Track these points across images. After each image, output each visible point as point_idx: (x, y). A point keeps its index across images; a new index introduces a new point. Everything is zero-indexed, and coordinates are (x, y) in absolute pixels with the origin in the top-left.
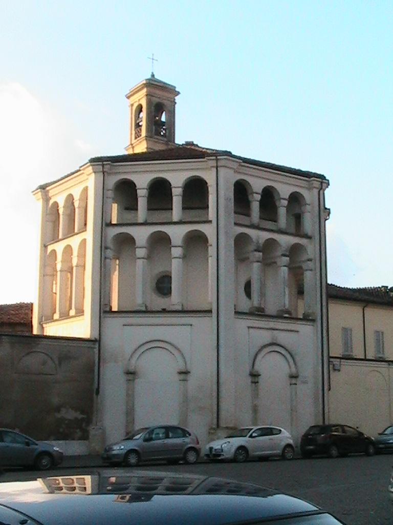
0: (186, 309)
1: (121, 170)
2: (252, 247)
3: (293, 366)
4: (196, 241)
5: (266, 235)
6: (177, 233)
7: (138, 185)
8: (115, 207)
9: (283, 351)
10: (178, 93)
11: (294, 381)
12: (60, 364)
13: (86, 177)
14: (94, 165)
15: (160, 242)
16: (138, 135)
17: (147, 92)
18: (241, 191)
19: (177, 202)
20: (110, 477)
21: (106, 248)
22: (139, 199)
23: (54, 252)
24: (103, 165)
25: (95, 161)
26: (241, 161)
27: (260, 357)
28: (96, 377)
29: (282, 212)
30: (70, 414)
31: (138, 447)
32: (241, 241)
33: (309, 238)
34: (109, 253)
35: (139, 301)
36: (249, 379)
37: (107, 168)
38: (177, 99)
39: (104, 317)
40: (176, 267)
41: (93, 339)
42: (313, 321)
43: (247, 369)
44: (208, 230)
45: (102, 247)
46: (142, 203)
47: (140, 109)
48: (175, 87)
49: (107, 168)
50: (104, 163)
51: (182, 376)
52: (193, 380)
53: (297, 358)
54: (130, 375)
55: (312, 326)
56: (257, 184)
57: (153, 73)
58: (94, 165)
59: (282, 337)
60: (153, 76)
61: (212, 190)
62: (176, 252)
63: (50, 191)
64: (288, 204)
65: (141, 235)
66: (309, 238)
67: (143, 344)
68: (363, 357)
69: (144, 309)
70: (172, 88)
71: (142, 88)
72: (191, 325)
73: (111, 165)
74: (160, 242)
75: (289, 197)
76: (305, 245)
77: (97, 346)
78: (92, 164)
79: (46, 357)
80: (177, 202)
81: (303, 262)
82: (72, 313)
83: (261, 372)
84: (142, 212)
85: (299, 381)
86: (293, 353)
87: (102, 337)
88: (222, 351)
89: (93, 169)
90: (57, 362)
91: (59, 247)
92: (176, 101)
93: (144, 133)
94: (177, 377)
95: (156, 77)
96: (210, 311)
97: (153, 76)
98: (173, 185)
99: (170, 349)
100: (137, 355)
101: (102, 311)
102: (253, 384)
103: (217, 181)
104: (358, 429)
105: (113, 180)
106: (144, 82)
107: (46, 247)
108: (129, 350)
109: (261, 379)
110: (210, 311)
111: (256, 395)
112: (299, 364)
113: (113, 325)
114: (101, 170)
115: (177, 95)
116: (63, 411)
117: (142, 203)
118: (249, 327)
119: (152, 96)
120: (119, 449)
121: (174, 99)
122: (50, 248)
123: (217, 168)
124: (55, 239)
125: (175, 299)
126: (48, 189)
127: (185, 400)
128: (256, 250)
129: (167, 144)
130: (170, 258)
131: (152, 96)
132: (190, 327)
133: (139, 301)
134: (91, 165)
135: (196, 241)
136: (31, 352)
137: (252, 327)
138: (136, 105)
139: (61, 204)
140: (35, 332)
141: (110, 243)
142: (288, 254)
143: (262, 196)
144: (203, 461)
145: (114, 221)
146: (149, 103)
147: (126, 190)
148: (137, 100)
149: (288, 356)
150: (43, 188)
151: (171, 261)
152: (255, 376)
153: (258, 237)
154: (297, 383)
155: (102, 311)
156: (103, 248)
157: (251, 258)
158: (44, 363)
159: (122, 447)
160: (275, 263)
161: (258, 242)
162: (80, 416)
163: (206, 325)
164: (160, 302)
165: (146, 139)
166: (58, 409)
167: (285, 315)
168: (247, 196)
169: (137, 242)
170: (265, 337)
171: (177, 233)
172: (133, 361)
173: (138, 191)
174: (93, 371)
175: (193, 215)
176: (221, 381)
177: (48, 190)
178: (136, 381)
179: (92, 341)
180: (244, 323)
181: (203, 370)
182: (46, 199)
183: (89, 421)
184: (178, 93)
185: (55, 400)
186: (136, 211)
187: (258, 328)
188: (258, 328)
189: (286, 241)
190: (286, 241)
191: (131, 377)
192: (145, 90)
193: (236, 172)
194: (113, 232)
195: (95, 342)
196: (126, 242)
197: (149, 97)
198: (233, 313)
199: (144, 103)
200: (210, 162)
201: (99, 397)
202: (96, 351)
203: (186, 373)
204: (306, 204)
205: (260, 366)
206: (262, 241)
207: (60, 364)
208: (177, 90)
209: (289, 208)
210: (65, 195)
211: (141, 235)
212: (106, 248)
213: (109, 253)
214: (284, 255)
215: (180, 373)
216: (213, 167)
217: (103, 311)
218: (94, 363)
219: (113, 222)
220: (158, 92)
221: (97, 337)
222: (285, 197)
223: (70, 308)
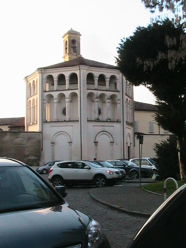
2: (95, 97)
3: (111, 138)
4: (74, 95)
5: (101, 92)
6: (67, 94)
7: (54, 77)
8: (47, 84)
9: (107, 134)
10: (81, 35)
11: (112, 144)
12: (28, 141)
13: (37, 75)
14: (39, 71)
15: (62, 96)
16: (66, 53)
17: (68, 36)
18: (90, 77)
19: (67, 82)
21: (44, 100)
22: (55, 82)
23: (30, 101)
24: (41, 70)
25: (38, 69)
27: (98, 136)
28: (41, 145)
30: (33, 158)
31: (47, 168)
32: (90, 95)
33: (119, 92)
34: (45, 101)
35: (55, 118)
36: (94, 144)
37: (43, 71)
38: (81, 37)
39: (44, 124)
40: (67, 105)
41: (40, 132)
42: (120, 122)
43: (93, 140)
44: (77, 92)
45: (42, 100)
46: (56, 83)
47: (66, 41)
48: (80, 33)
49: (43, 71)
50: (42, 70)
51: (70, 144)
52: (73, 144)
53: (113, 136)
54: (52, 144)
55: (120, 124)
56: (97, 73)
58: (39, 71)
59: (106, 129)
60: (72, 29)
61: (79, 77)
62: (67, 100)
63: (28, 79)
64: (110, 80)
65: (55, 94)
66: (119, 92)
68: (158, 134)
69: (57, 121)
70: (78, 33)
71: (66, 35)
72: (72, 126)
73: (45, 70)
74: (62, 96)
75: (110, 77)
76: (117, 95)
77: (41, 133)
78: (38, 70)
79: (23, 139)
80: (67, 82)
81: (116, 101)
82: (31, 124)
83: (98, 141)
84: (56, 86)
85: (114, 144)
86: (111, 134)
87: (43, 131)
88: (82, 135)
89: (38, 72)
90: (27, 140)
91: (31, 99)
92: (80, 38)
93: (68, 52)
94: (109, 144)
95: (73, 29)
96: (78, 121)
97: (72, 29)
98: (66, 76)
99: (66, 135)
100: (55, 136)
101: (43, 122)
102: (95, 146)
103: (80, 74)
105: (46, 75)
106: (67, 32)
107: (28, 99)
108: (52, 135)
109: (98, 144)
110: (78, 121)
111: (96, 149)
112: (114, 138)
113: (47, 126)
114: (41, 72)
115: (80, 36)
116: (30, 156)
117: (56, 83)
118: (93, 126)
119: (70, 37)
121: (80, 38)
122: (29, 99)
123: (80, 69)
124: (31, 96)
126: (27, 78)
127: (71, 152)
128: (96, 98)
129: (76, 55)
130: (65, 102)
131: (70, 37)
132: (72, 127)
133: (55, 118)
134: (38, 71)
135: (74, 95)
136: (18, 137)
137: (95, 126)
138: (65, 41)
139: (32, 84)
140: (26, 131)
141: (45, 98)
142: (109, 98)
143: (99, 78)
144: (152, 181)
145: (47, 90)
146: (69, 40)
147: (50, 78)
148: (65, 39)
149: (109, 135)
150: (26, 78)
151: (65, 104)
152: (96, 143)
153: (97, 93)
154: (114, 145)
155: (43, 122)
156: (43, 100)
157: (95, 101)
158: (22, 141)
159: (41, 168)
161: (97, 95)
162: (36, 158)
163: (78, 124)
164: (63, 118)
165: (68, 55)
166: (28, 156)
167: (109, 121)
168: (93, 78)
169: (54, 97)
170: (101, 129)
171: (67, 94)
172: (54, 139)
174: (41, 143)
175: (73, 86)
176: (82, 145)
177: (27, 79)
178: (55, 145)
179: (40, 132)
180: (91, 124)
181: (76, 141)
182: (27, 81)
183: (39, 160)
184: (81, 35)
185: (27, 153)
186: (53, 86)
187: (97, 126)
188: (97, 126)
189: (109, 94)
190: (109, 94)
191: (53, 144)
192: (67, 36)
193: (87, 70)
194: (46, 94)
195: (41, 132)
196: (51, 97)
197: (69, 38)
198: (87, 121)
199: (67, 40)
200: (77, 68)
201: (43, 151)
202: (41, 136)
203: (71, 142)
204: (117, 79)
205: (99, 139)
206: (99, 95)
207: (28, 141)
208: (81, 34)
209: (110, 82)
211: (55, 94)
212: (44, 100)
213: (45, 101)
214: (108, 99)
215: (111, 143)
216: (78, 69)
217: (44, 122)
218: (41, 140)
219: (47, 90)
220: (72, 36)
221: (41, 131)
222: (108, 78)
223: (35, 121)
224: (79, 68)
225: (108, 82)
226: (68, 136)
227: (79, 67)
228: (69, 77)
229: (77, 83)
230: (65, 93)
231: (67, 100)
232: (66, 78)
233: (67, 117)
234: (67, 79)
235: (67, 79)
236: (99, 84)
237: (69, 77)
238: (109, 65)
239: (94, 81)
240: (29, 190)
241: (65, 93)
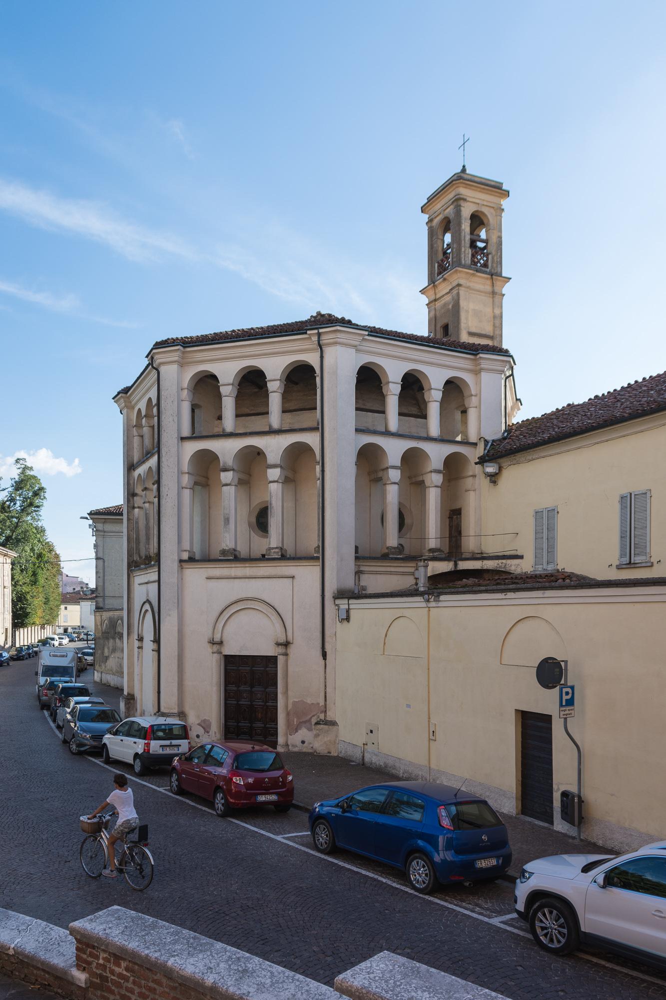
0: (298, 556)
1: (200, 356)
7: (269, 376)
19: (275, 401)
20: (476, 860)
26: (367, 333)
29: (434, 410)
57: (464, 166)
60: (464, 170)
67: (236, 602)
72: (293, 577)
80: (275, 401)
97: (464, 170)
104: (75, 591)
120: (145, 722)
125: (274, 540)
132: (288, 581)
160: (423, 482)
164: (260, 545)
173: (221, 388)
175: (292, 420)
186: (357, 427)
210: (145, 400)
224: (319, 338)
225: (438, 404)
226: (274, 617)
227: (319, 335)
228: (237, 383)
229: (315, 409)
230: (219, 447)
231: (274, 474)
232: (269, 385)
233: (274, 540)
234: (275, 387)
235: (275, 387)
236: (405, 411)
237: (280, 380)
238: (275, 325)
239: (382, 398)
240: (295, 723)
241: (219, 447)
